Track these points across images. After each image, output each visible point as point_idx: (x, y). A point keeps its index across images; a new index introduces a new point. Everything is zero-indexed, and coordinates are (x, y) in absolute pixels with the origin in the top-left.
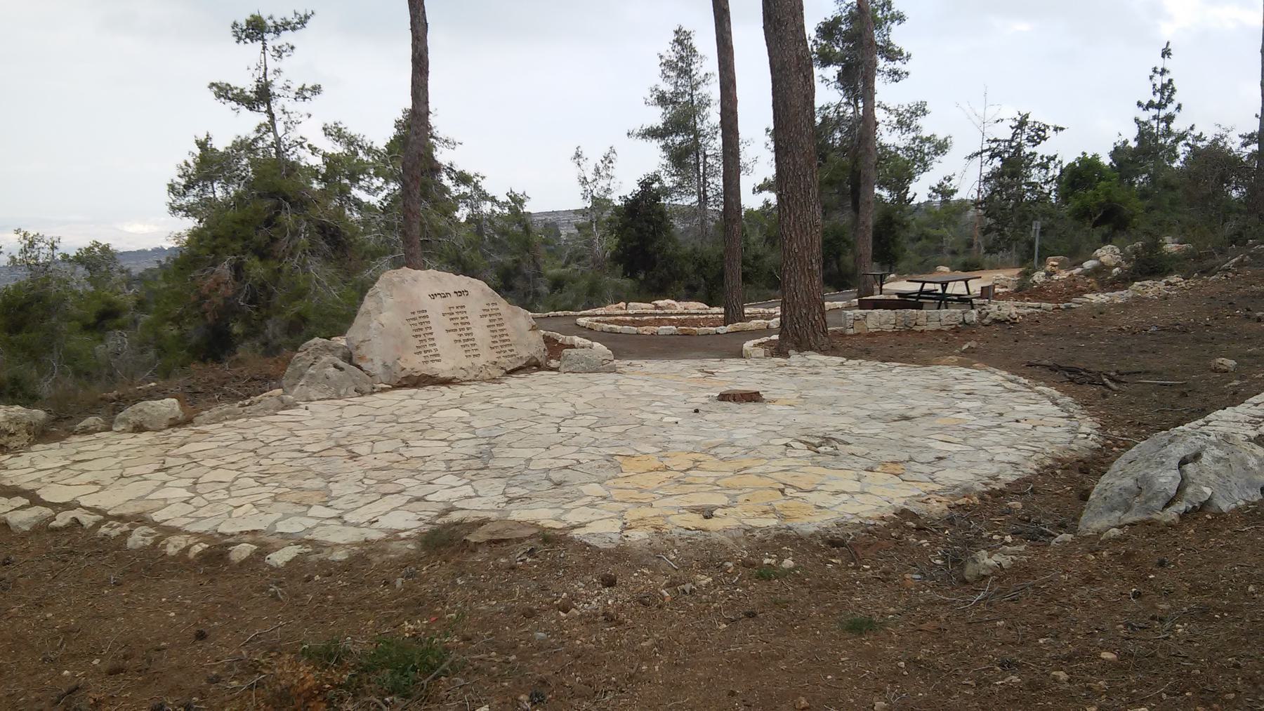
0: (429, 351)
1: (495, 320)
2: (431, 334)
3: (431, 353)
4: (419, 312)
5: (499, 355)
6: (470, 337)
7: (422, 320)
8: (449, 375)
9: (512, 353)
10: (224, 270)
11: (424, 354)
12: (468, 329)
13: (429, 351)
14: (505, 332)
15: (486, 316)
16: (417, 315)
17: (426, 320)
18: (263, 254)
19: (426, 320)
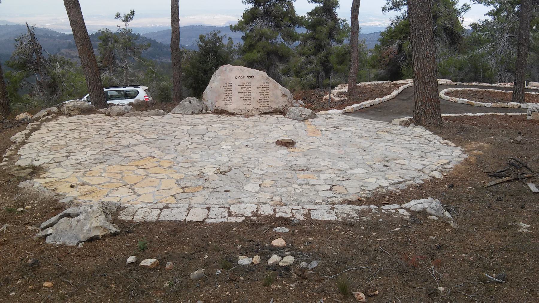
0: (228, 100)
2: (231, 93)
3: (229, 101)
4: (229, 83)
5: (261, 105)
6: (249, 96)
7: (229, 87)
9: (268, 105)
10: (394, 47)
11: (226, 101)
12: (249, 93)
13: (228, 100)
14: (268, 96)
15: (260, 88)
16: (227, 85)
17: (231, 87)
19: (231, 87)
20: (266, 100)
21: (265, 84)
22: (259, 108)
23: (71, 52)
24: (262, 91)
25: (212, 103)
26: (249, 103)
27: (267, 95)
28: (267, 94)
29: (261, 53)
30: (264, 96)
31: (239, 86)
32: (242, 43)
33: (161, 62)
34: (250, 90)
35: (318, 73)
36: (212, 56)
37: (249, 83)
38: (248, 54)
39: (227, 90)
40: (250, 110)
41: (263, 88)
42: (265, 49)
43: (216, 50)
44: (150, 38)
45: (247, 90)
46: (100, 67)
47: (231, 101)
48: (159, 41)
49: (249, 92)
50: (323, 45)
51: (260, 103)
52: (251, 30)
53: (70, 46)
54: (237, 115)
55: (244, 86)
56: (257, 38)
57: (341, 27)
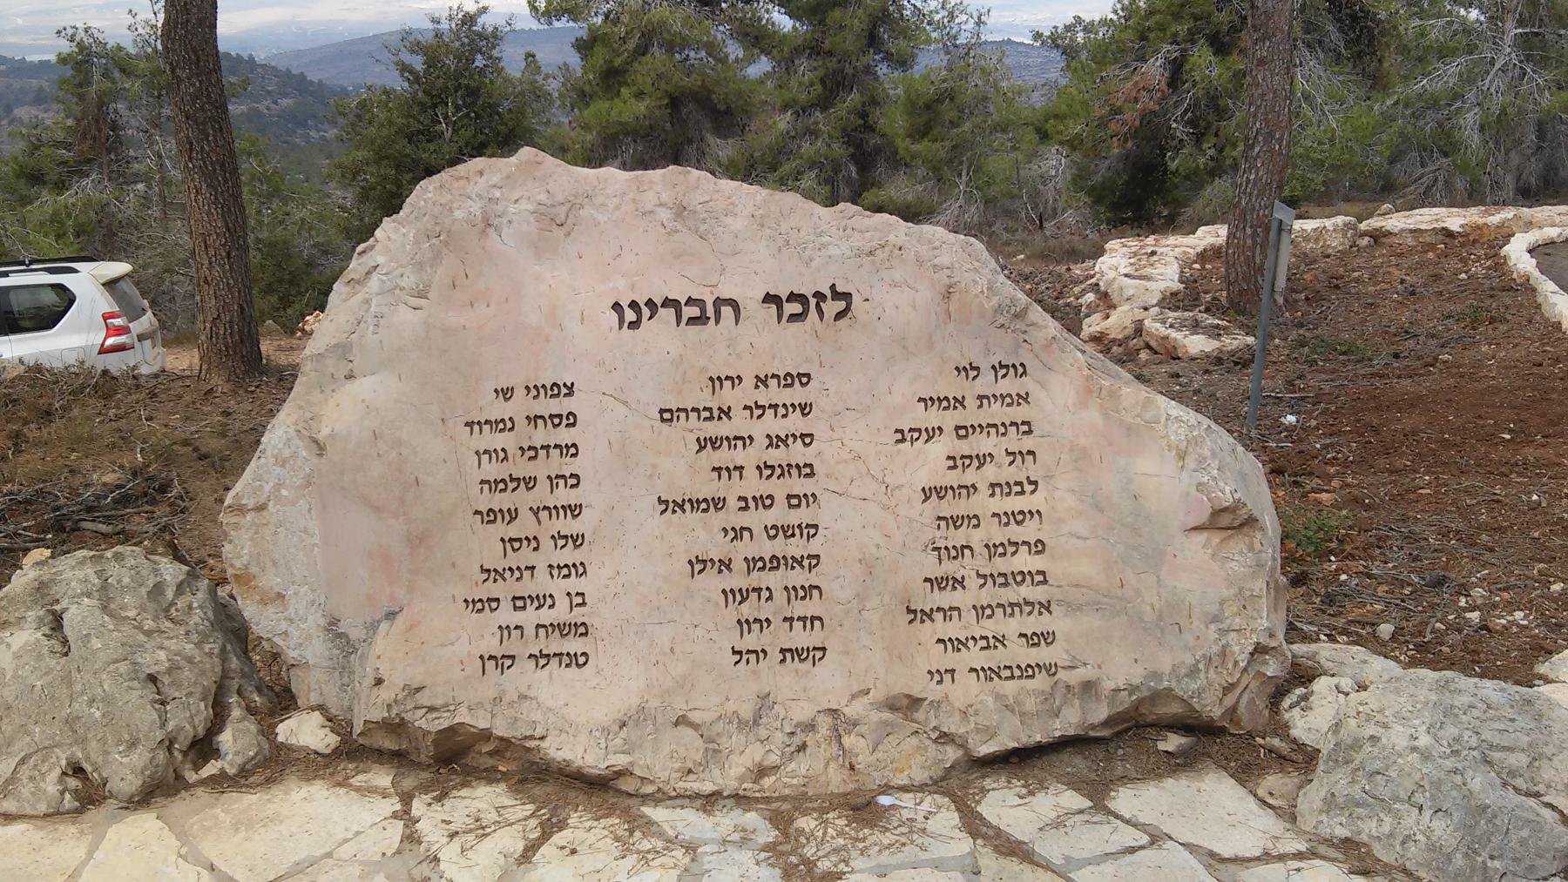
0: (541, 601)
1: (982, 460)
2: (574, 510)
3: (546, 616)
4: (535, 390)
5: (950, 659)
6: (796, 547)
7: (541, 436)
8: (588, 756)
9: (1043, 654)
10: (1154, 69)
11: (506, 615)
12: (795, 501)
13: (541, 601)
14: (1029, 531)
15: (932, 434)
16: (519, 407)
17: (564, 436)
18: (1221, 46)
19: (564, 436)
20: (1005, 580)
21: (985, 384)
22: (932, 691)
23: (45, 115)
24: (953, 478)
25: (332, 627)
26: (801, 638)
27: (1019, 517)
28: (1015, 503)
29: (648, 101)
30: (977, 538)
31: (667, 415)
32: (574, 60)
33: (323, 138)
34: (808, 471)
35: (836, 169)
36: (458, 108)
37: (789, 380)
38: (601, 105)
39: (522, 468)
40: (824, 723)
41: (962, 431)
42: (663, 86)
43: (473, 84)
44: (287, 69)
45: (767, 470)
46: (65, 163)
47: (578, 615)
48: (313, 76)
49: (799, 486)
50: (849, 70)
51: (942, 628)
52: (607, 16)
53: (40, 99)
54: (659, 798)
55: (726, 413)
56: (631, 45)
57: (908, 13)
